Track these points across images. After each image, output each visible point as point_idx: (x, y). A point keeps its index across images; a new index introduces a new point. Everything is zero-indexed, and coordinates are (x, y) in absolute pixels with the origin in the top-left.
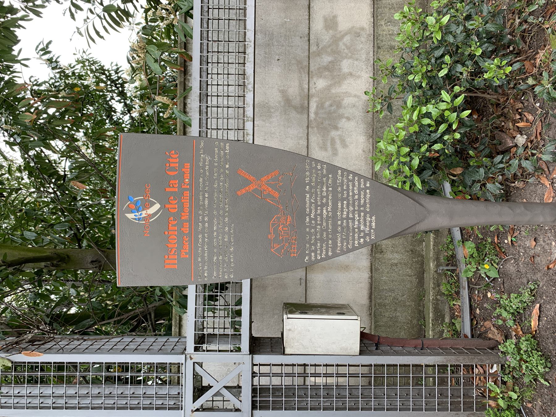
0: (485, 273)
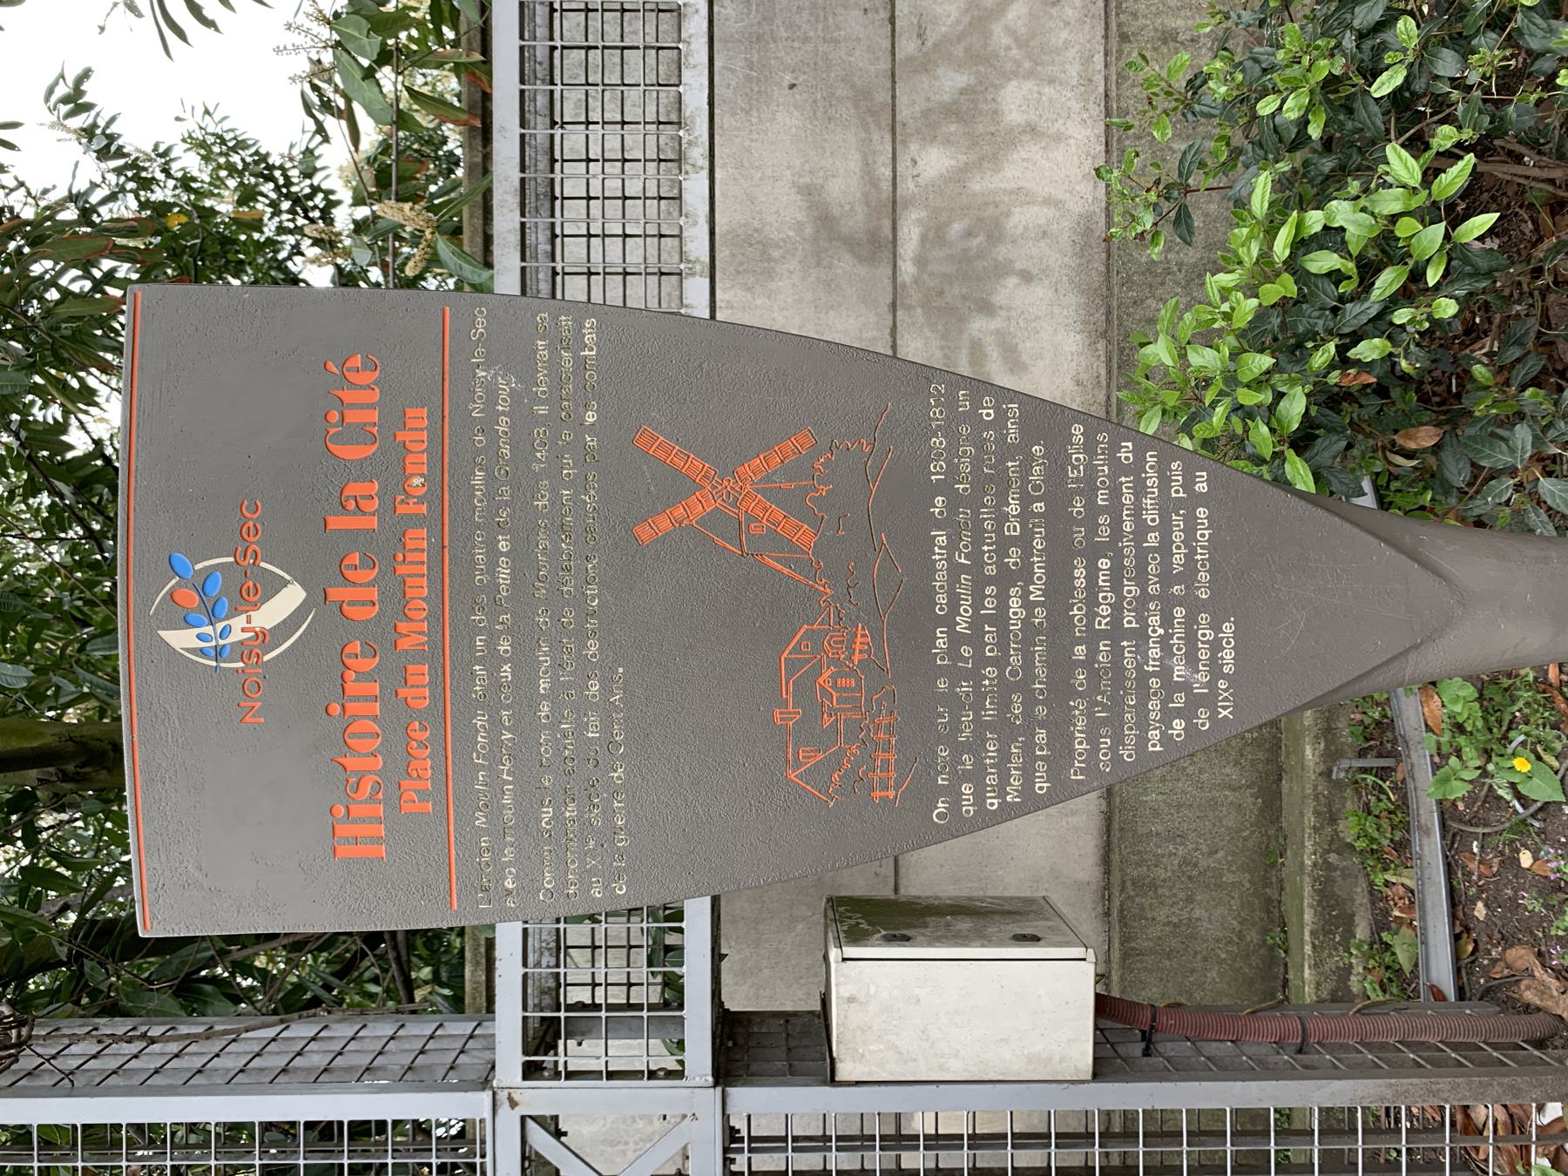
0: (1513, 786)
